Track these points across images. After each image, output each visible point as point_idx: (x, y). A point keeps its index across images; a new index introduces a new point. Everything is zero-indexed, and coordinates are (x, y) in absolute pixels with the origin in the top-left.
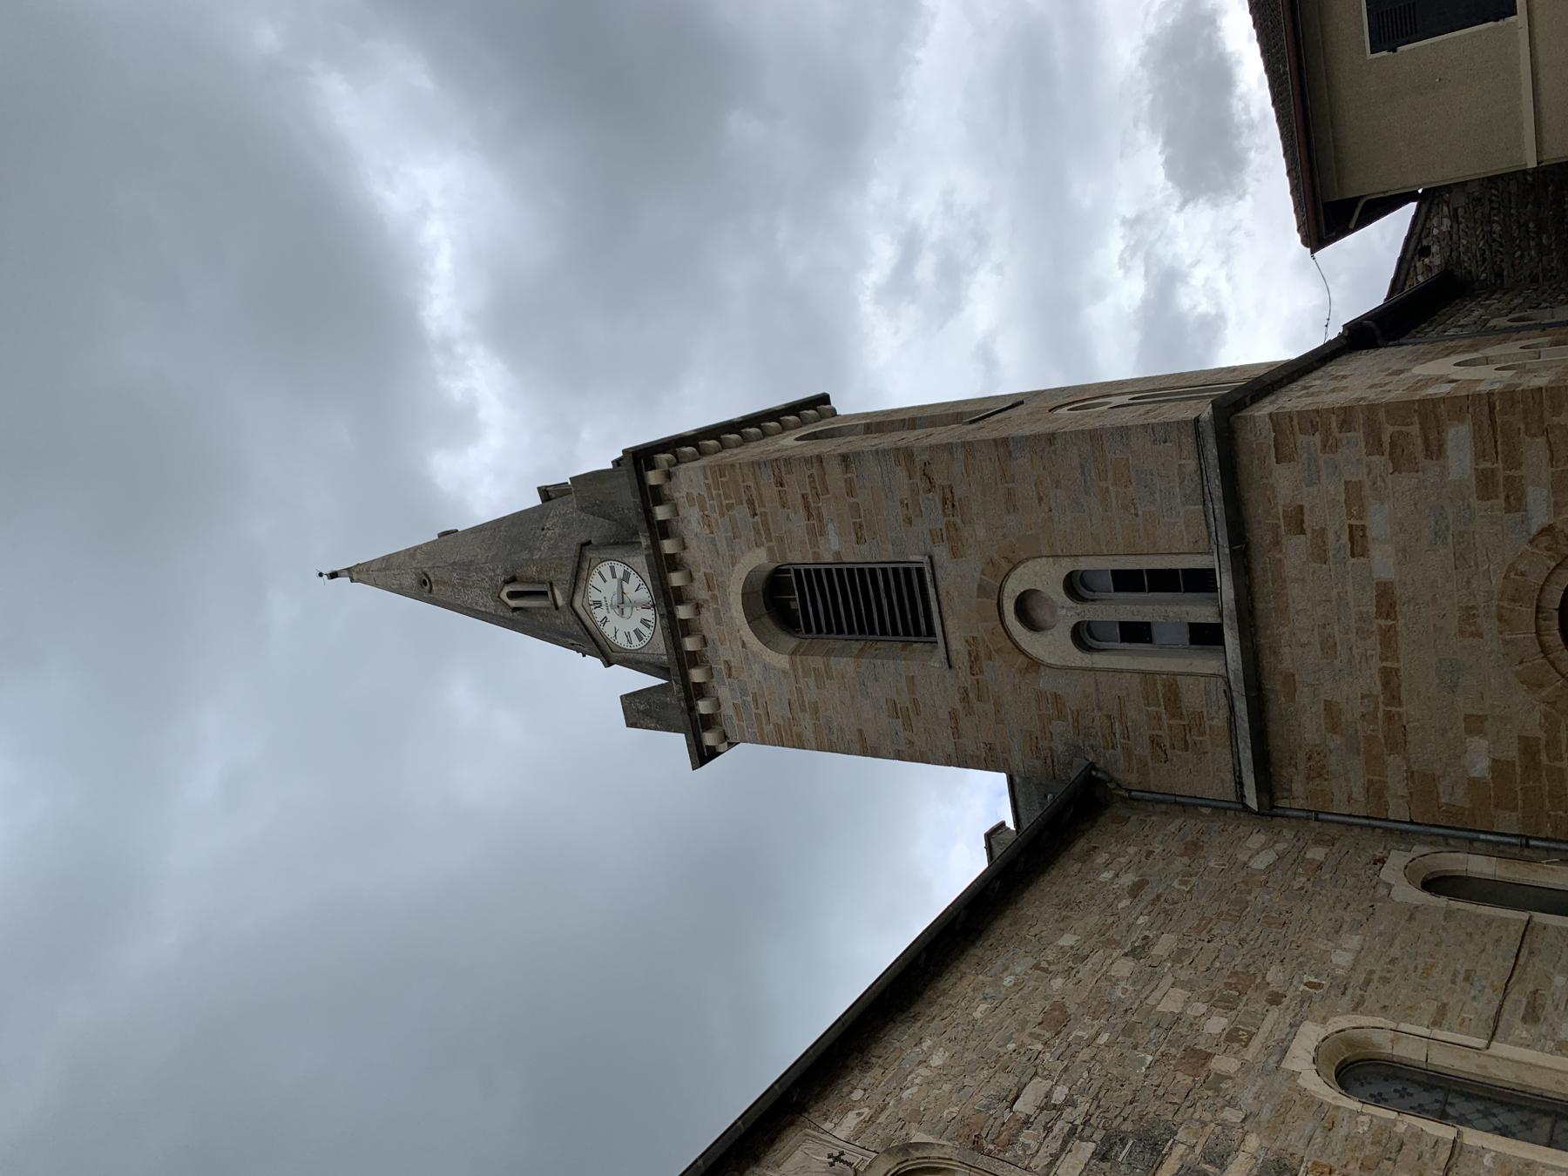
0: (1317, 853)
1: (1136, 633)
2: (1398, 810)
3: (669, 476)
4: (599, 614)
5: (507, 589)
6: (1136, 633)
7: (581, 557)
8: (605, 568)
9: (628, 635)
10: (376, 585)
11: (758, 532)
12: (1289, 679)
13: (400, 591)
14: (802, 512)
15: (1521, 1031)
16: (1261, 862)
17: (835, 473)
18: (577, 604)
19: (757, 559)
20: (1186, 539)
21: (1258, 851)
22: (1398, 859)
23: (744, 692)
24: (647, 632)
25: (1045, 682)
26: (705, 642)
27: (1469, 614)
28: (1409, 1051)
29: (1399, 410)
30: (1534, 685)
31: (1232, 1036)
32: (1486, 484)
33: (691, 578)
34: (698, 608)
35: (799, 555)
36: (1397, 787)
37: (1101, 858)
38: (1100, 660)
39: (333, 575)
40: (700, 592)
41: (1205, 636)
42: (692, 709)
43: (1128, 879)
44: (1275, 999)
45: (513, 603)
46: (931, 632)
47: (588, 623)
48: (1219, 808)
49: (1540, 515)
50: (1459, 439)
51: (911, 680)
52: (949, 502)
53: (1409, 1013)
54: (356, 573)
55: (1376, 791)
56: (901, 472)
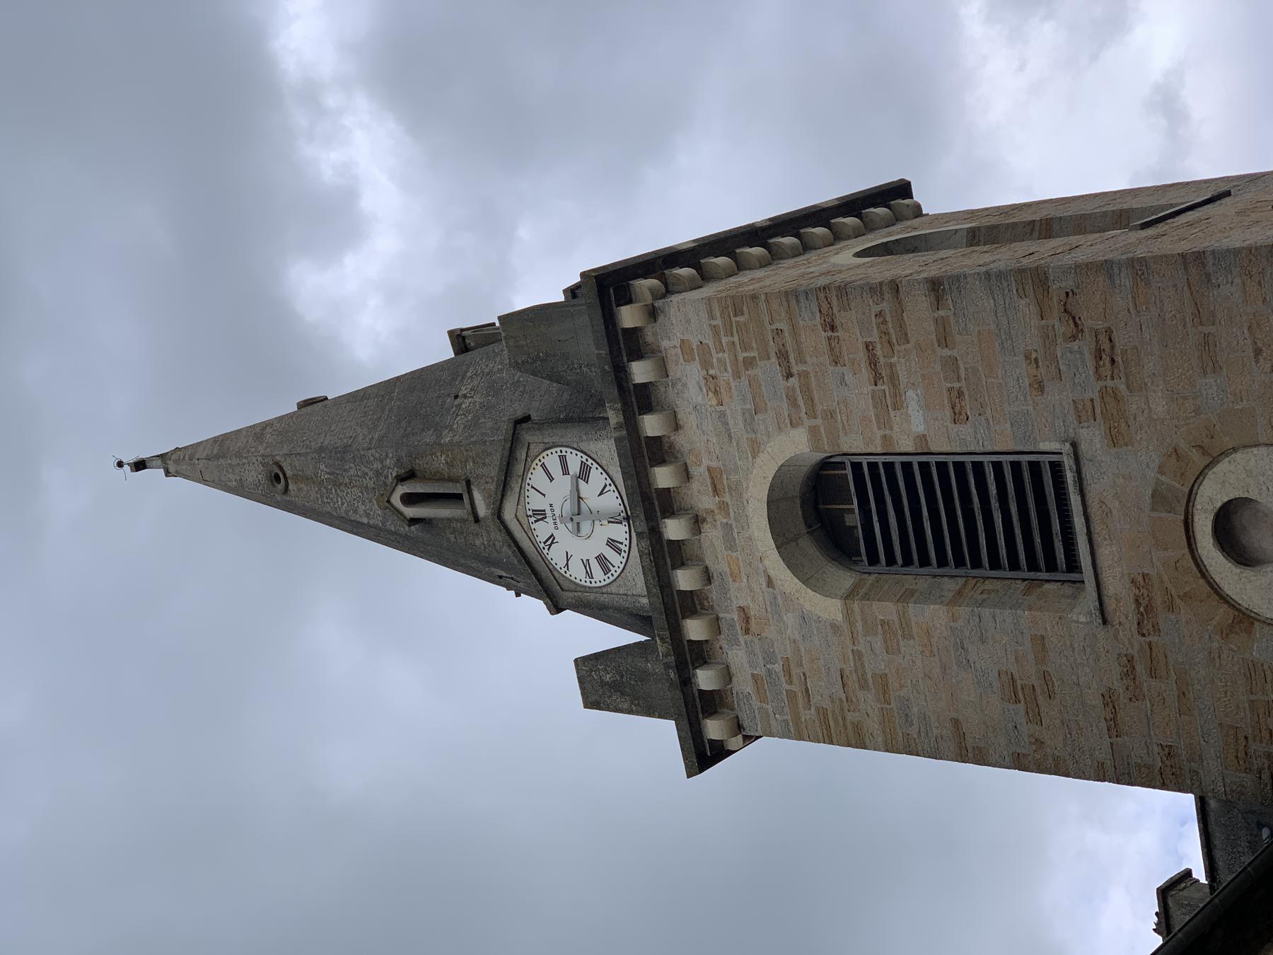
4: (542, 531)
5: (402, 489)
8: (551, 459)
9: (586, 564)
11: (793, 403)
14: (866, 373)
17: (919, 308)
18: (508, 515)
19: (792, 446)
23: (770, 658)
24: (616, 560)
35: (860, 440)
39: (140, 465)
42: (686, 681)
46: (1073, 565)
51: (1040, 642)
56: (1026, 308)
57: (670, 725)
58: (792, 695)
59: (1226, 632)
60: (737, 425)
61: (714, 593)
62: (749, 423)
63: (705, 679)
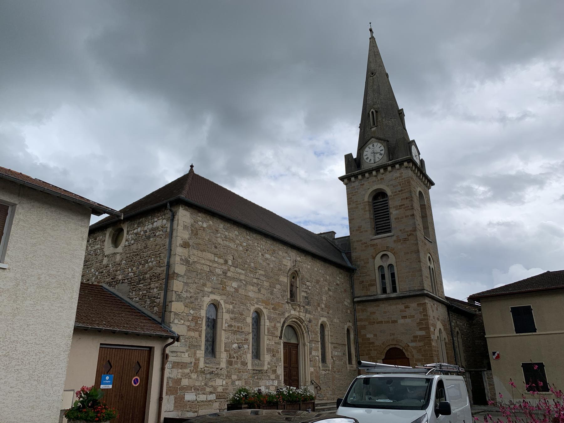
0: (349, 312)
1: (383, 277)
2: (359, 323)
3: (406, 167)
4: (371, 146)
5: (374, 111)
6: (383, 277)
7: (385, 140)
8: (382, 148)
9: (367, 155)
10: (370, 50)
11: (395, 192)
12: (379, 306)
13: (369, 62)
14: (400, 204)
15: (332, 347)
16: (346, 303)
17: (409, 213)
18: (373, 139)
19: (389, 193)
20: (403, 287)
21: (347, 302)
22: (350, 324)
23: (358, 189)
24: (368, 161)
25: (371, 260)
26: (368, 178)
27: (393, 334)
28: (326, 333)
29: (427, 324)
30: (383, 344)
31: (322, 309)
32: (416, 337)
33: (382, 174)
34: (376, 176)
35: (391, 203)
36: (363, 323)
37: (340, 276)
38: (377, 271)
39: (371, 30)
40: (380, 176)
41: (384, 291)
42: (352, 176)
43: (338, 282)
44: (328, 313)
45: (370, 113)
46: (378, 234)
47: (368, 143)
48: (353, 293)
49: (410, 344)
50: (423, 333)
51: (367, 231)
52: (405, 240)
53: (331, 332)
54: (372, 39)
55: (361, 320)
56: (411, 229)
57: (345, 174)
58: (353, 193)
59: (372, 256)
60: (391, 183)
61: (365, 179)
62: (391, 185)
63: (353, 179)
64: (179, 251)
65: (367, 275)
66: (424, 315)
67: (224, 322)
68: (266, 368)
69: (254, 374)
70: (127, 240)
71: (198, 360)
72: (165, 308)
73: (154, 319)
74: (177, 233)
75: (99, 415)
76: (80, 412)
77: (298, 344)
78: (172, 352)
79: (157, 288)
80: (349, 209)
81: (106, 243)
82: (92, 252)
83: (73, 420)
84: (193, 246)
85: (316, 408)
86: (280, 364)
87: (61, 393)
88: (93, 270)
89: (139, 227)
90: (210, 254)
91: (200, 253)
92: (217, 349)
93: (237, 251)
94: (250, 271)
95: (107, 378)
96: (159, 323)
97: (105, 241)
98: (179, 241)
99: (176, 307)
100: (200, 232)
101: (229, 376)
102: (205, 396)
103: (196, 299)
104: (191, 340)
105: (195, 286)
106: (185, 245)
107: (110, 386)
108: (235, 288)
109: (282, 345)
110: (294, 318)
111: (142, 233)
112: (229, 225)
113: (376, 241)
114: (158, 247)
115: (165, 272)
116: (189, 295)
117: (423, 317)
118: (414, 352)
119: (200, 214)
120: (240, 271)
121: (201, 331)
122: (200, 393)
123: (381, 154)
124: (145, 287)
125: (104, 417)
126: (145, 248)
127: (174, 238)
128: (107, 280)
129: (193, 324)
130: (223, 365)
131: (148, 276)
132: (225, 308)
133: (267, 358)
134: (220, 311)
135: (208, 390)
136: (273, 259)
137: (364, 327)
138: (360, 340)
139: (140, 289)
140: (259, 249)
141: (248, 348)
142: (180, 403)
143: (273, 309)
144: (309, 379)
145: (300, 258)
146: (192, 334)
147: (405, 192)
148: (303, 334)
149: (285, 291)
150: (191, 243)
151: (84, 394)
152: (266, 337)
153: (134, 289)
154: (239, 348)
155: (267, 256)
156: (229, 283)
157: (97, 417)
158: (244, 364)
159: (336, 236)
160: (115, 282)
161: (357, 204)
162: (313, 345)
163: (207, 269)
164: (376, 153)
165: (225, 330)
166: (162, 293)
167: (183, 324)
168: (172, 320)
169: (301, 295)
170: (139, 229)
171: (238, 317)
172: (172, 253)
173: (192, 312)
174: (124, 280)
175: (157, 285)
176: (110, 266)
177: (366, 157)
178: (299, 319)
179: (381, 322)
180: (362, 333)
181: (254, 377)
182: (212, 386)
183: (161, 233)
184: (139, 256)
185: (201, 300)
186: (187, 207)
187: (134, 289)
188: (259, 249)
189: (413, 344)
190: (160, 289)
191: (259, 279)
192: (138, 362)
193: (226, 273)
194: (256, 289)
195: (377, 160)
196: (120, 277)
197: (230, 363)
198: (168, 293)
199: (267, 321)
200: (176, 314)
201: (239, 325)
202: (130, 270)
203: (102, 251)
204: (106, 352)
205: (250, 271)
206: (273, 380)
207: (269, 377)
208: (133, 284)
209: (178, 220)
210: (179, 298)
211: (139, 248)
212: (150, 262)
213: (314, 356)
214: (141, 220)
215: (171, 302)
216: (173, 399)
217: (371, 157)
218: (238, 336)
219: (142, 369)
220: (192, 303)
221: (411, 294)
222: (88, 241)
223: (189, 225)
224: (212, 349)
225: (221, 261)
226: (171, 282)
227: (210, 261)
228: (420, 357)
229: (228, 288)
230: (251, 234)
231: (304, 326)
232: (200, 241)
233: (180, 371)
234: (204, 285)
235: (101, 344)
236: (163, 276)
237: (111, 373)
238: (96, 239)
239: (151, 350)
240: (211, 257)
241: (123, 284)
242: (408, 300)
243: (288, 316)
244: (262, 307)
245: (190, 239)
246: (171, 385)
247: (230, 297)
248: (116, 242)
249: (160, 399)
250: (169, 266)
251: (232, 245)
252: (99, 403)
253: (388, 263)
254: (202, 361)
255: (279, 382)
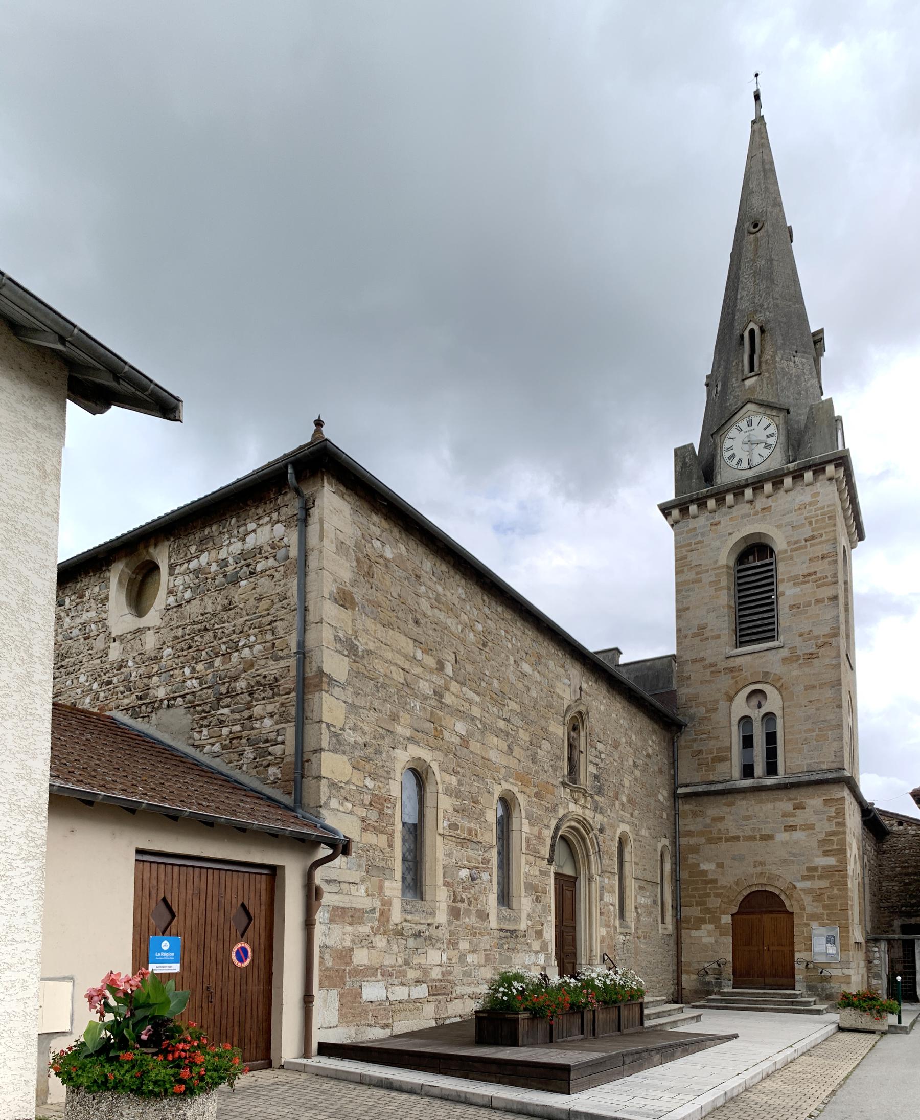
0: (665, 816)
1: (748, 742)
2: (683, 841)
4: (743, 424)
5: (756, 328)
6: (748, 742)
7: (780, 409)
8: (773, 429)
9: (731, 448)
11: (796, 543)
12: (733, 804)
14: (806, 572)
16: (661, 798)
18: (750, 406)
19: (780, 544)
20: (791, 762)
21: (663, 795)
23: (703, 535)
25: (723, 704)
26: (730, 507)
27: (762, 864)
30: (737, 883)
31: (623, 805)
32: (815, 869)
35: (783, 570)
36: (693, 841)
37: (654, 738)
38: (735, 729)
39: (757, 97)
40: (761, 502)
41: (748, 771)
43: (650, 751)
44: (632, 815)
45: (746, 334)
46: (742, 644)
48: (674, 777)
49: (799, 885)
50: (831, 861)
51: (718, 637)
52: (811, 656)
54: (759, 122)
55: (690, 834)
56: (827, 630)
58: (690, 544)
59: (727, 694)
60: (787, 519)
63: (693, 508)
64: (329, 612)
65: (710, 738)
66: (838, 824)
67: (441, 815)
68: (523, 926)
69: (501, 938)
70: (170, 592)
71: (387, 903)
72: (303, 768)
73: (269, 798)
74: (320, 558)
75: (185, 1073)
76: (110, 1060)
77: (576, 878)
78: (328, 882)
79: (272, 715)
80: (677, 584)
81: (111, 604)
82: (76, 632)
83: (89, 1090)
84: (363, 607)
85: (646, 1012)
86: (549, 918)
87: (32, 990)
88: (82, 679)
89: (203, 551)
90: (403, 638)
91: (381, 632)
92: (428, 879)
93: (463, 641)
94: (491, 698)
95: (165, 945)
96: (287, 807)
97: (107, 598)
98: (329, 587)
99: (332, 765)
100: (378, 570)
101: (453, 944)
102: (405, 989)
103: (378, 752)
104: (370, 853)
105: (373, 716)
106: (344, 600)
107: (176, 968)
108: (461, 737)
109: (553, 876)
110: (579, 822)
111: (214, 567)
112: (444, 568)
113: (739, 661)
114: (264, 604)
115: (293, 672)
116: (361, 740)
117: (834, 828)
118: (807, 900)
119: (375, 518)
120: (471, 694)
121: (391, 835)
122: (396, 982)
123: (767, 446)
124: (237, 716)
125: (202, 1079)
126: (226, 609)
127: (312, 576)
128: (126, 701)
129: (373, 815)
130: (442, 917)
131: (241, 685)
132: (443, 783)
133: (525, 903)
134: (430, 788)
135: (412, 974)
136: (538, 677)
137: (695, 849)
138: (684, 875)
139: (222, 722)
140: (510, 646)
141: (490, 879)
142: (351, 1006)
143: (537, 795)
144: (597, 952)
145: (589, 685)
146: (371, 838)
147: (821, 543)
148: (588, 855)
149: (558, 758)
150: (357, 598)
151: (117, 999)
152: (523, 856)
153: (205, 722)
154: (473, 879)
155: (526, 667)
156: (448, 721)
157: (181, 1081)
158: (483, 916)
159: (623, 660)
160: (147, 705)
161: (697, 574)
162: (606, 881)
163: (399, 677)
164: (753, 444)
165: (443, 835)
166: (290, 731)
167: (351, 813)
168: (323, 799)
169: (587, 770)
170: (204, 558)
171: (469, 807)
172: (311, 617)
173: (369, 783)
174: (174, 698)
175: (270, 708)
176: (130, 663)
177: (730, 453)
178: (583, 822)
179: (737, 838)
180: (690, 861)
181: (502, 945)
182: (420, 966)
183: (271, 562)
184: (211, 633)
185: (389, 756)
186: (342, 488)
187: (205, 722)
188: (510, 646)
189: (807, 884)
190: (283, 718)
191: (508, 721)
192: (243, 905)
193: (441, 696)
194: (504, 745)
195: (757, 460)
196: (161, 693)
197: (455, 913)
198: (307, 727)
199: (525, 821)
200: (332, 785)
201: (472, 825)
202: (187, 671)
203: (104, 625)
204: (154, 874)
205: (491, 698)
206: (537, 952)
207: (530, 947)
208: (202, 709)
209: (321, 521)
210: (339, 745)
211: (209, 610)
212: (244, 646)
213: (607, 905)
214: (207, 531)
215: (319, 750)
216: (337, 998)
217: (741, 453)
218: (471, 853)
219: (255, 922)
220: (368, 760)
221: (812, 778)
222: (60, 604)
223: (350, 543)
224: (415, 882)
225: (430, 662)
226: (314, 698)
227: (406, 656)
228: (820, 911)
229: (446, 735)
230: (493, 604)
231: (591, 839)
232: (379, 596)
233: (349, 929)
234: (394, 718)
235: (139, 851)
236: (288, 683)
237: (174, 931)
238: (82, 596)
239: (274, 873)
240: (407, 645)
241: (172, 711)
242: (804, 791)
243: (564, 816)
244: (515, 790)
245: (355, 583)
246: (329, 964)
247: (451, 756)
248: (138, 600)
249: (307, 999)
250: (303, 653)
251: (451, 622)
252: (178, 1029)
253: (763, 711)
254: (397, 905)
255: (547, 958)
